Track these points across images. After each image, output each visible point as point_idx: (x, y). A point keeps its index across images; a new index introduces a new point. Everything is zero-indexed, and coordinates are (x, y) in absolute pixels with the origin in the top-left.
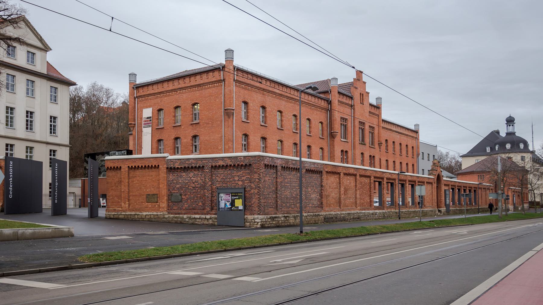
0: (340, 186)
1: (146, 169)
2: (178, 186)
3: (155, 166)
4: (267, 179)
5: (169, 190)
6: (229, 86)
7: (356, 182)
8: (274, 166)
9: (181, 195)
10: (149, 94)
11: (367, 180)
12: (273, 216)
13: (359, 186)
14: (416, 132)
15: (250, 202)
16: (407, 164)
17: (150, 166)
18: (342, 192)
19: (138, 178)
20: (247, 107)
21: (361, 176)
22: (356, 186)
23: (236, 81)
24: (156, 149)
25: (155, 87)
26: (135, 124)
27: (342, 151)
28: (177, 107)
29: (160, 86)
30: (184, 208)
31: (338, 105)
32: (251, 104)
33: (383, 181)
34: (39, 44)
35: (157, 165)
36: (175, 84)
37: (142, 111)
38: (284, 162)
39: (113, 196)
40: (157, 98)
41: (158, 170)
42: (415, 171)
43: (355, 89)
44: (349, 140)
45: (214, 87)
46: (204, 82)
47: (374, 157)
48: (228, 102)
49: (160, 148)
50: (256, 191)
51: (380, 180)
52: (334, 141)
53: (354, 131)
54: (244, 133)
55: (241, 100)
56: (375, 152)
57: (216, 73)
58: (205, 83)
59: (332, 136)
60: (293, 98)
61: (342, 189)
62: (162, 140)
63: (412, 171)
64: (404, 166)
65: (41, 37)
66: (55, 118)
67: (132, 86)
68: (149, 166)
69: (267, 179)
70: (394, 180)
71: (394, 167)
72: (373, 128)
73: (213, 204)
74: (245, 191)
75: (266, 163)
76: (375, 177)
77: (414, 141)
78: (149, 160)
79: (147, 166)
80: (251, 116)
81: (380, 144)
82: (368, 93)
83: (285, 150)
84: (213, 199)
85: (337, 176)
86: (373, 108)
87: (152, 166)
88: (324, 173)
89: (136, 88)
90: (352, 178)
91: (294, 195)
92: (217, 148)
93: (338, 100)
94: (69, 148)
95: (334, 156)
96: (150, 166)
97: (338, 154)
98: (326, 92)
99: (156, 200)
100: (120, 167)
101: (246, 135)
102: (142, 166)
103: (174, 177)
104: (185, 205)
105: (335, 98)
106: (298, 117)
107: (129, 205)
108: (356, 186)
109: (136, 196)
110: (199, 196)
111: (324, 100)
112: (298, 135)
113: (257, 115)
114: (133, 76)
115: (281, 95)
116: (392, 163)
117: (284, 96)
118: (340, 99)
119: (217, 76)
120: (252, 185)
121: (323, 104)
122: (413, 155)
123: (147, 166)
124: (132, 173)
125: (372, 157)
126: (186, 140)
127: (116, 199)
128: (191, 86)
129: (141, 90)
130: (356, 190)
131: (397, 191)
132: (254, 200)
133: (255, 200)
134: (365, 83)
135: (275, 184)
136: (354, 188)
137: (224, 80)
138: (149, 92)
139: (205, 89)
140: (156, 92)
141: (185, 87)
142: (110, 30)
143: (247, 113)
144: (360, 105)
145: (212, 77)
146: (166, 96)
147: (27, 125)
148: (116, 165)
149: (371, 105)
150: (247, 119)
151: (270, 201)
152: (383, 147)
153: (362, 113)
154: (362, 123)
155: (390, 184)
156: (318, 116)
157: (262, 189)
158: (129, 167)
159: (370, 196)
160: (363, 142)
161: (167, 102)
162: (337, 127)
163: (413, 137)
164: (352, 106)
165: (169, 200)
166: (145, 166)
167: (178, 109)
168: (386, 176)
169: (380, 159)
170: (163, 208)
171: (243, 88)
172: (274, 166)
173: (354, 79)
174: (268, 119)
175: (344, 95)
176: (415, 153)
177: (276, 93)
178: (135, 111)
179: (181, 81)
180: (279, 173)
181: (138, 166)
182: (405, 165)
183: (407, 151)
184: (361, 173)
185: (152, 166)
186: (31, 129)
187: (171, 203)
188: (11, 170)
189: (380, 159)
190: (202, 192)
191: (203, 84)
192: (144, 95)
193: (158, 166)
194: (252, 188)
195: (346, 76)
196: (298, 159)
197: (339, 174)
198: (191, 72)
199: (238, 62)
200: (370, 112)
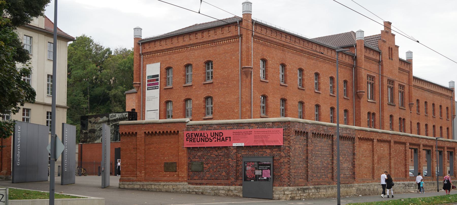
0: (373, 155)
1: (165, 136)
3: (174, 132)
4: (297, 146)
5: (189, 158)
6: (247, 42)
7: (390, 149)
8: (304, 132)
9: (202, 163)
10: (156, 51)
11: (401, 148)
12: (305, 187)
13: (393, 154)
14: (452, 90)
15: (280, 172)
16: (441, 127)
17: (169, 132)
18: (376, 161)
20: (266, 65)
21: (396, 143)
22: (390, 154)
23: (255, 37)
24: (164, 113)
25: (163, 43)
26: (140, 84)
27: (369, 113)
28: (187, 66)
29: (169, 41)
30: (206, 178)
31: (365, 61)
32: (270, 62)
33: (420, 148)
35: (176, 131)
36: (186, 40)
38: (315, 128)
41: (177, 136)
42: (450, 136)
43: (383, 43)
44: (377, 101)
45: (230, 43)
46: (218, 38)
47: (404, 119)
48: (245, 59)
50: (286, 160)
51: (416, 147)
52: (359, 102)
53: (382, 91)
54: (263, 94)
55: (259, 57)
56: (406, 114)
57: (232, 28)
58: (220, 39)
59: (358, 96)
60: (315, 54)
61: (376, 157)
62: (170, 101)
63: (424, 133)
64: (438, 129)
67: (138, 42)
68: (167, 132)
69: (297, 146)
70: (432, 146)
71: (427, 131)
72: (403, 86)
73: (238, 174)
74: (273, 160)
75: (297, 129)
76: (411, 144)
77: (449, 101)
78: (167, 125)
79: (165, 132)
80: (270, 75)
81: (411, 105)
82: (398, 47)
83: (306, 113)
84: (238, 168)
85: (303, 138)
86: (403, 63)
87: (171, 132)
88: (357, 140)
89: (142, 43)
90: (386, 146)
91: (325, 165)
92: (233, 111)
93: (365, 56)
94: (66, 110)
95: (360, 119)
96: (169, 132)
97: (364, 116)
98: (351, 47)
99: (174, 168)
100: (136, 133)
101: (265, 97)
102: (160, 132)
104: (208, 175)
105: (360, 53)
106: (336, 79)
107: (145, 174)
108: (390, 154)
109: (153, 164)
110: (222, 165)
111: (349, 55)
112: (336, 98)
113: (294, 79)
116: (424, 127)
117: (305, 51)
118: (367, 55)
119: (233, 31)
120: (282, 153)
121: (348, 60)
122: (448, 117)
123: (165, 132)
125: (402, 120)
126: (197, 101)
128: (204, 42)
129: (147, 47)
130: (390, 159)
131: (435, 160)
132: (284, 170)
133: (284, 170)
134: (394, 35)
135: (305, 152)
136: (388, 156)
137: (241, 35)
138: (156, 49)
139: (219, 45)
140: (164, 48)
141: (197, 43)
142: (199, 13)
143: (266, 72)
144: (389, 60)
145: (227, 33)
146: (174, 53)
148: (131, 131)
149: (401, 60)
150: (266, 79)
151: (300, 171)
152: (414, 108)
153: (391, 71)
154: (391, 82)
155: (413, 150)
156: (343, 75)
157: (293, 158)
158: (145, 132)
159: (406, 165)
160: (392, 103)
161: (177, 60)
162: (365, 88)
163: (447, 96)
164: (380, 62)
165: (189, 169)
166: (163, 132)
168: (422, 143)
169: (411, 122)
170: (183, 177)
171: (261, 44)
172: (304, 132)
173: (382, 31)
174: (288, 78)
175: (370, 49)
176: (450, 115)
177: (297, 49)
178: (140, 69)
179: (192, 37)
180: (310, 140)
181: (156, 132)
182: (439, 128)
183: (441, 112)
184: (396, 140)
185: (171, 132)
187: (191, 173)
189: (411, 122)
190: (226, 160)
191: (218, 39)
192: (151, 52)
193: (178, 131)
194: (281, 157)
195: (373, 29)
196: (336, 124)
197: (372, 140)
198: (204, 27)
199: (256, 17)
200: (400, 69)
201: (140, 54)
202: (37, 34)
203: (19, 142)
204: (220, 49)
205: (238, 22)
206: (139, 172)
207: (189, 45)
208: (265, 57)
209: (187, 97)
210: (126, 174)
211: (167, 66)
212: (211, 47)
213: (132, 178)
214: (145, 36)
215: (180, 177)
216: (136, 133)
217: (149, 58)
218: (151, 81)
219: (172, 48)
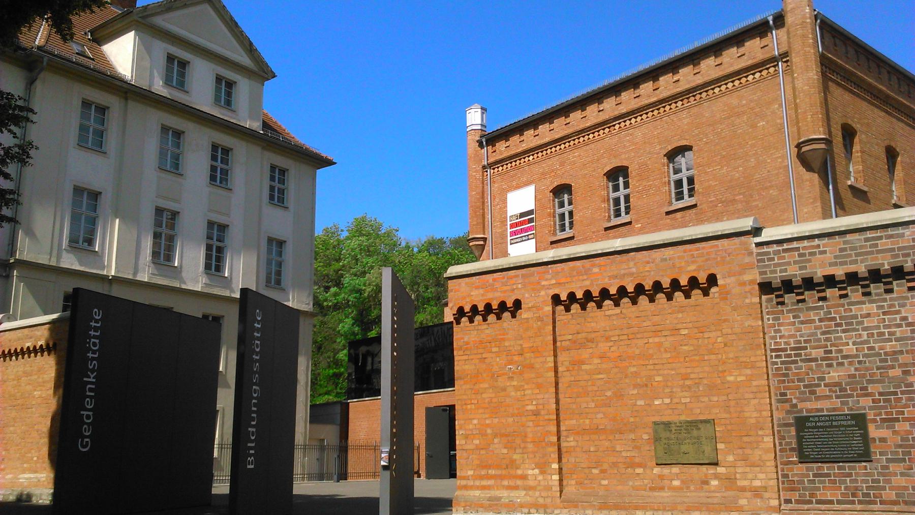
2: (834, 375)
5: (783, 398)
19: (603, 346)
26: (485, 239)
34: (244, 59)
35: (702, 278)
37: (505, 201)
39: (483, 434)
45: (746, 86)
65: (251, 44)
66: (281, 243)
99: (708, 449)
103: (806, 330)
109: (596, 430)
124: (571, 322)
127: (499, 448)
129: (501, 146)
138: (524, 146)
139: (709, 99)
140: (547, 140)
158: (556, 299)
170: (757, 493)
188: (94, 343)
202: (244, 144)
204: (714, 107)
206: (538, 466)
208: (850, 122)
210: (481, 478)
211: (556, 184)
212: (683, 109)
213: (504, 494)
215: (743, 489)
217: (507, 172)
218: (517, 225)
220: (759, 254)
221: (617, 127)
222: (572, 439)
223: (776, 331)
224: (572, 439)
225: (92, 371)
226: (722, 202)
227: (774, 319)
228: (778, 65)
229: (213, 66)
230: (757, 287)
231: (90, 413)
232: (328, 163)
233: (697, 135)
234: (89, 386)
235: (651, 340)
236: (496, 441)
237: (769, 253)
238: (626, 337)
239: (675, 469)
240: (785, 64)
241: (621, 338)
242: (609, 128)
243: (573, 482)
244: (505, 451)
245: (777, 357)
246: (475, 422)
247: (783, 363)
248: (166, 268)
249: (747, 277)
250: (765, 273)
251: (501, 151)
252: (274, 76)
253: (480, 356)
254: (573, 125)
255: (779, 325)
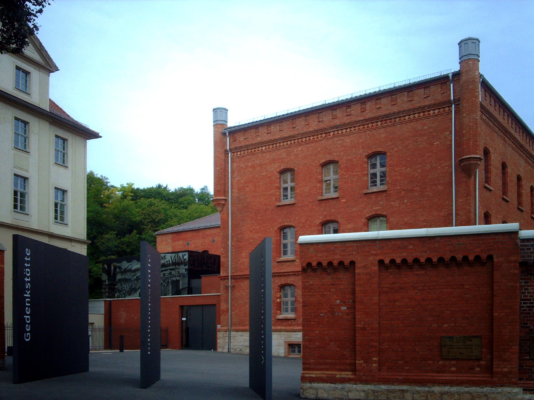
10: (260, 143)
36: (325, 119)
40: (277, 149)
49: (284, 242)
66: (64, 192)
73: (489, 357)
94: (86, 247)
100: (352, 263)
107: (380, 364)
114: (220, 114)
115: (522, 146)
138: (259, 139)
139: (401, 123)
140: (277, 137)
147: (15, 200)
158: (381, 262)
167: (332, 167)
186: (22, 208)
192: (247, 146)
201: (226, 151)
203: (28, 286)
205: (450, 75)
207: (332, 128)
209: (328, 218)
211: (282, 167)
212: (383, 127)
214: (233, 122)
216: (352, 263)
217: (243, 156)
219: (293, 136)
220: (521, 246)
221: (332, 134)
222: (386, 344)
223: (525, 289)
224: (386, 344)
225: (28, 290)
226: (404, 190)
227: (525, 283)
228: (452, 106)
229: (14, 60)
230: (518, 264)
231: (29, 317)
232: (94, 135)
233: (390, 146)
234: (27, 300)
235: (444, 290)
236: (331, 343)
237: (528, 245)
238: (427, 288)
239: (453, 362)
240: (232, 154)
241: (424, 288)
242: (325, 133)
243: (385, 368)
244: (338, 349)
245: (524, 303)
246: (317, 332)
247: (527, 307)
248: (21, 215)
249: (513, 258)
250: (524, 257)
251: (240, 142)
252: (58, 70)
253: (321, 293)
254: (298, 129)
255: (528, 286)
